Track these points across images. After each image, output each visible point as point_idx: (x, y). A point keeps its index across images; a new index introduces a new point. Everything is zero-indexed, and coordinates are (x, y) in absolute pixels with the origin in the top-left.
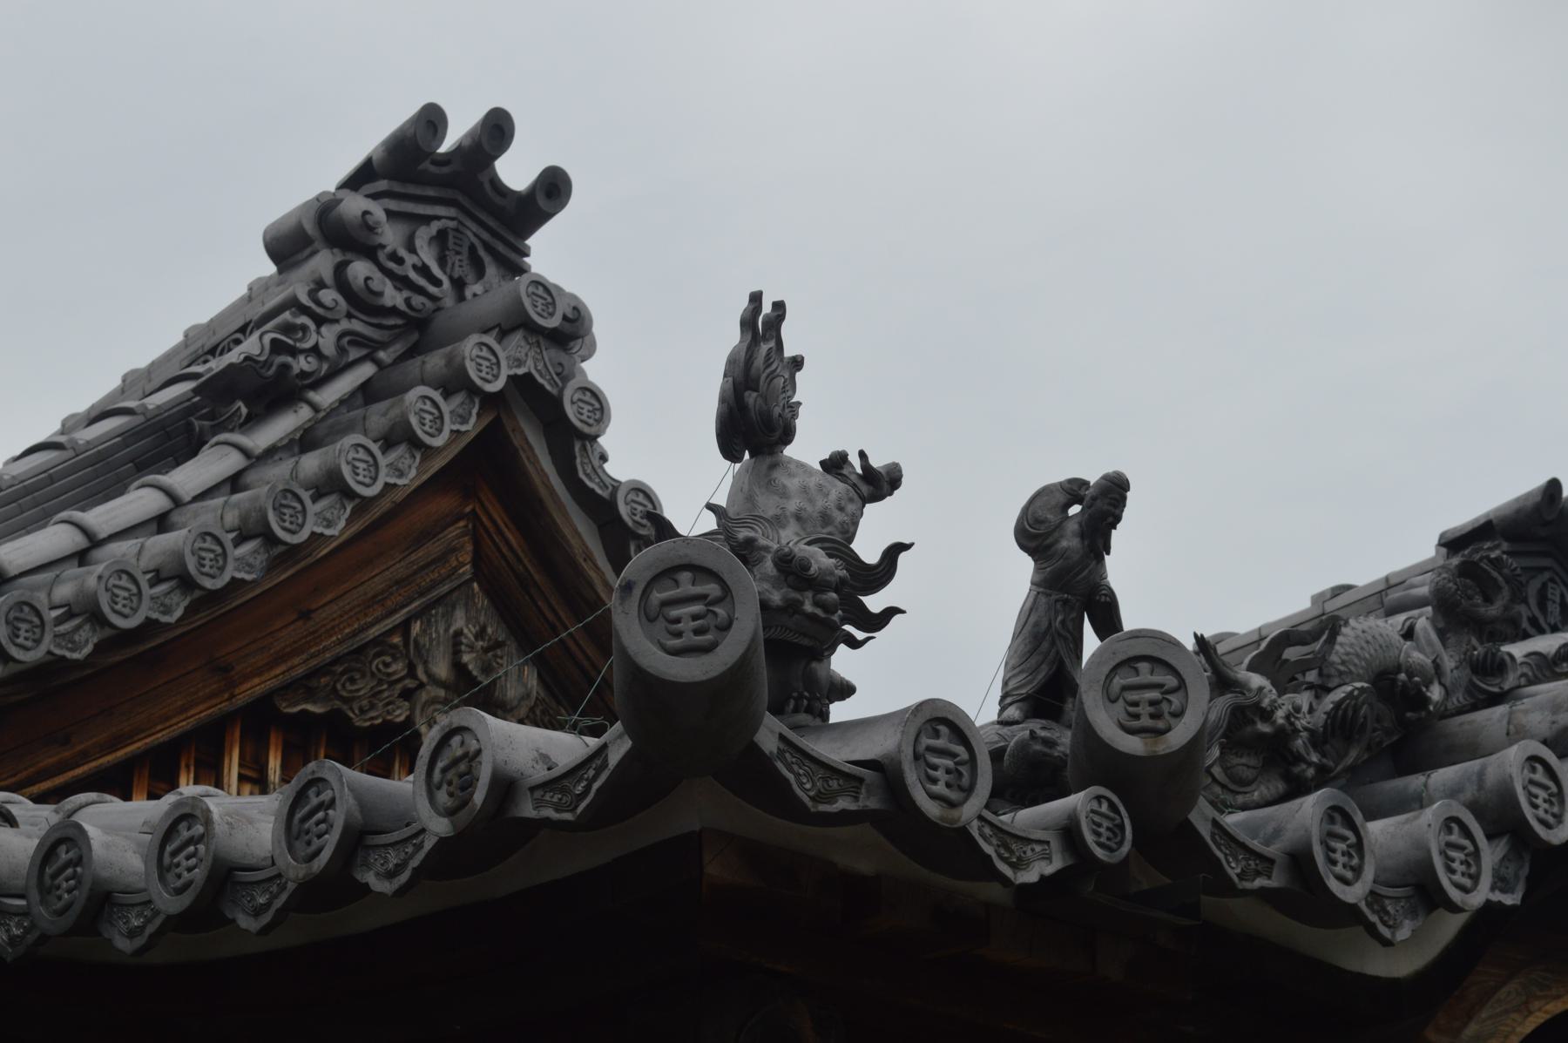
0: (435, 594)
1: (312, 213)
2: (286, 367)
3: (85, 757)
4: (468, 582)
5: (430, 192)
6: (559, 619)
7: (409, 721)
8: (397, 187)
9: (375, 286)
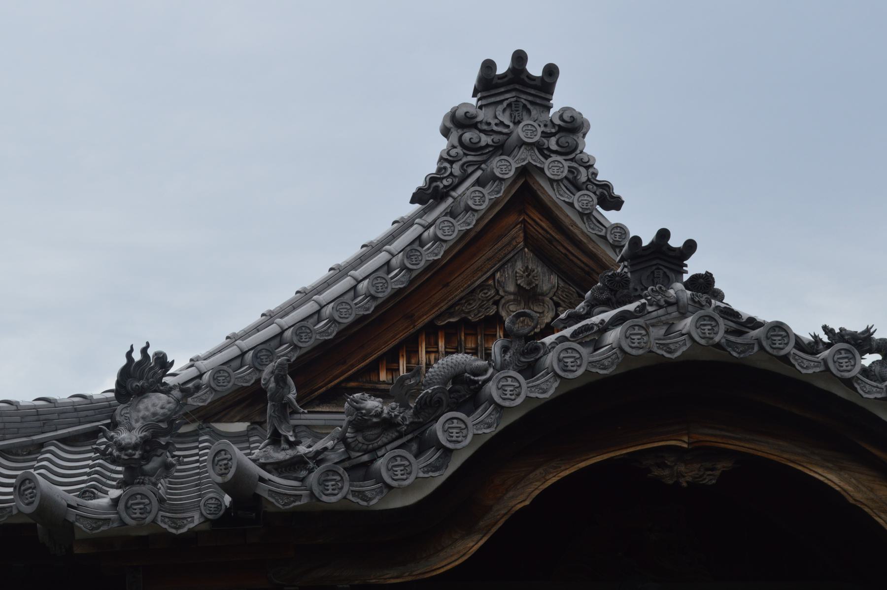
0: (505, 260)
1: (449, 118)
2: (437, 187)
3: (353, 366)
4: (522, 249)
5: (502, 90)
6: (568, 250)
7: (497, 312)
8: (485, 94)
9: (475, 140)
